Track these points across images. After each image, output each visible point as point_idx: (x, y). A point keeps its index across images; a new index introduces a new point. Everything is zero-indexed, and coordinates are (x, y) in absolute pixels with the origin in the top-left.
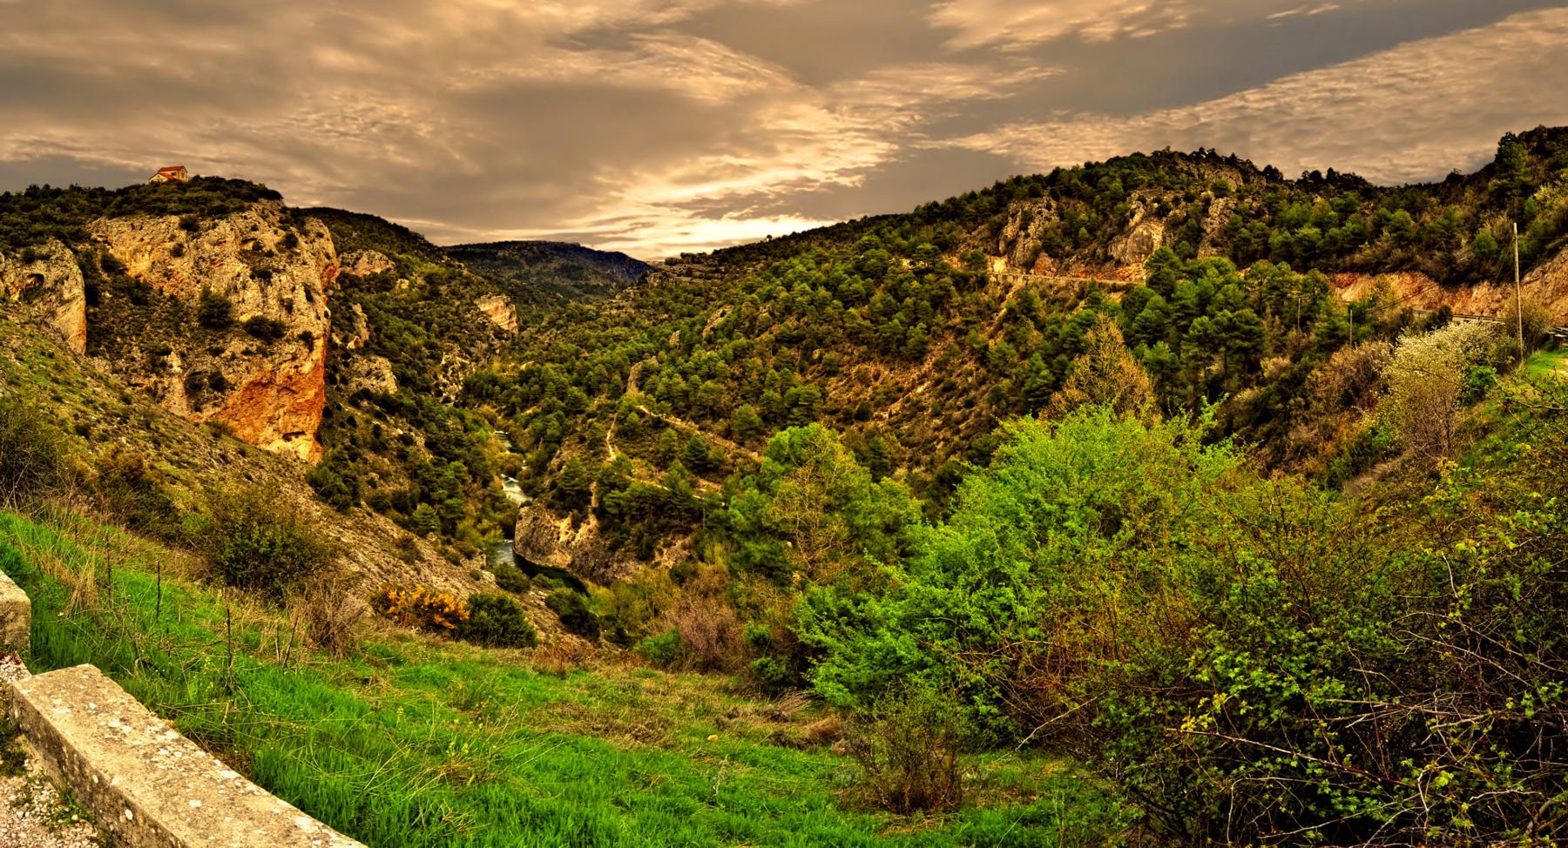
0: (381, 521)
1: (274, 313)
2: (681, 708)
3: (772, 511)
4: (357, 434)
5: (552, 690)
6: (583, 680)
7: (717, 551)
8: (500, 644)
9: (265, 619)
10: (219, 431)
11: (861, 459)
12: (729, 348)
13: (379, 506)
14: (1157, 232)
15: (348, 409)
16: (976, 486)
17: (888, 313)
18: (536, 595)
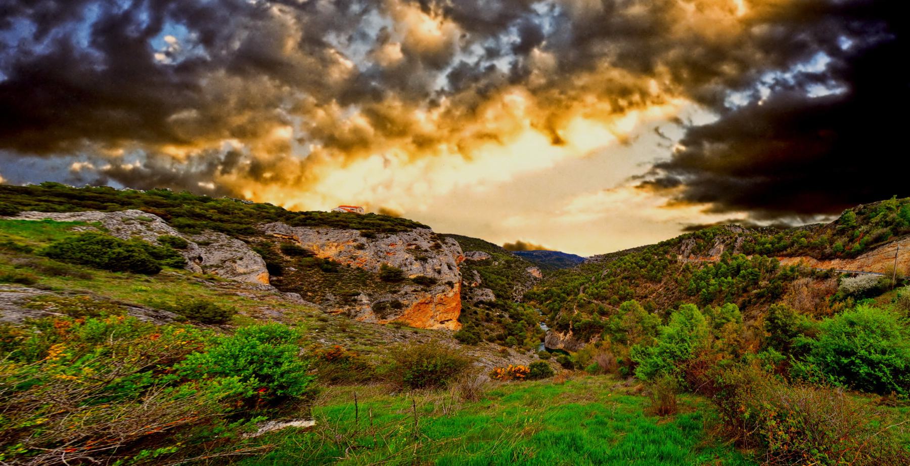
0: (492, 345)
1: (430, 274)
2: (599, 387)
3: (622, 324)
4: (478, 317)
5: (559, 390)
6: (570, 383)
7: (608, 338)
8: (541, 378)
9: (436, 397)
10: (398, 326)
11: (645, 308)
12: (609, 281)
13: (491, 340)
14: (722, 247)
15: (474, 308)
16: (675, 315)
17: (652, 270)
18: (553, 359)
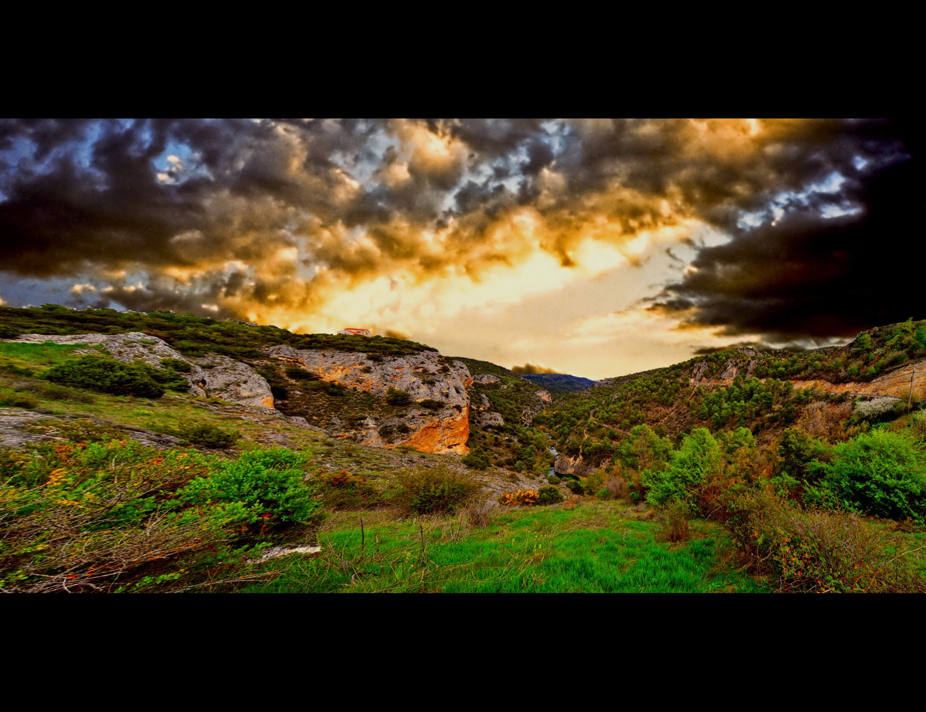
0: (501, 470)
1: (438, 398)
2: (610, 512)
3: (633, 449)
4: (487, 441)
5: (569, 515)
6: (580, 509)
7: (618, 462)
8: (551, 503)
9: (444, 523)
10: (405, 450)
11: (657, 433)
12: (620, 404)
13: (500, 465)
14: (735, 370)
15: (482, 432)
16: (687, 440)
17: (663, 394)
18: (563, 484)
